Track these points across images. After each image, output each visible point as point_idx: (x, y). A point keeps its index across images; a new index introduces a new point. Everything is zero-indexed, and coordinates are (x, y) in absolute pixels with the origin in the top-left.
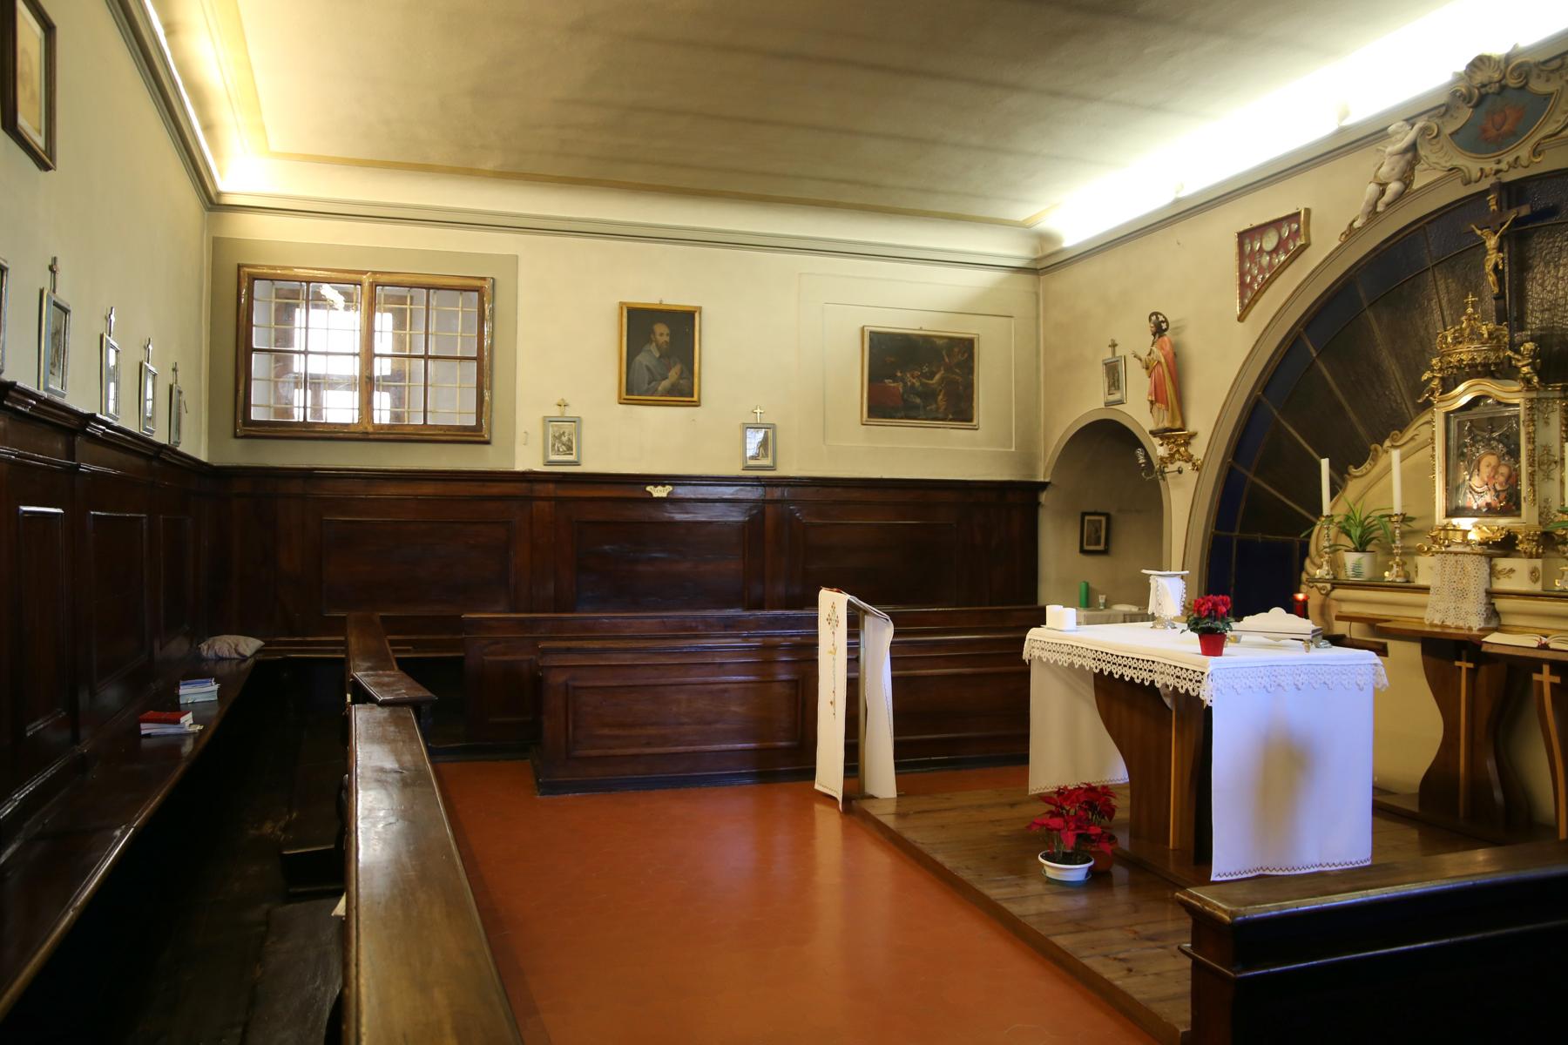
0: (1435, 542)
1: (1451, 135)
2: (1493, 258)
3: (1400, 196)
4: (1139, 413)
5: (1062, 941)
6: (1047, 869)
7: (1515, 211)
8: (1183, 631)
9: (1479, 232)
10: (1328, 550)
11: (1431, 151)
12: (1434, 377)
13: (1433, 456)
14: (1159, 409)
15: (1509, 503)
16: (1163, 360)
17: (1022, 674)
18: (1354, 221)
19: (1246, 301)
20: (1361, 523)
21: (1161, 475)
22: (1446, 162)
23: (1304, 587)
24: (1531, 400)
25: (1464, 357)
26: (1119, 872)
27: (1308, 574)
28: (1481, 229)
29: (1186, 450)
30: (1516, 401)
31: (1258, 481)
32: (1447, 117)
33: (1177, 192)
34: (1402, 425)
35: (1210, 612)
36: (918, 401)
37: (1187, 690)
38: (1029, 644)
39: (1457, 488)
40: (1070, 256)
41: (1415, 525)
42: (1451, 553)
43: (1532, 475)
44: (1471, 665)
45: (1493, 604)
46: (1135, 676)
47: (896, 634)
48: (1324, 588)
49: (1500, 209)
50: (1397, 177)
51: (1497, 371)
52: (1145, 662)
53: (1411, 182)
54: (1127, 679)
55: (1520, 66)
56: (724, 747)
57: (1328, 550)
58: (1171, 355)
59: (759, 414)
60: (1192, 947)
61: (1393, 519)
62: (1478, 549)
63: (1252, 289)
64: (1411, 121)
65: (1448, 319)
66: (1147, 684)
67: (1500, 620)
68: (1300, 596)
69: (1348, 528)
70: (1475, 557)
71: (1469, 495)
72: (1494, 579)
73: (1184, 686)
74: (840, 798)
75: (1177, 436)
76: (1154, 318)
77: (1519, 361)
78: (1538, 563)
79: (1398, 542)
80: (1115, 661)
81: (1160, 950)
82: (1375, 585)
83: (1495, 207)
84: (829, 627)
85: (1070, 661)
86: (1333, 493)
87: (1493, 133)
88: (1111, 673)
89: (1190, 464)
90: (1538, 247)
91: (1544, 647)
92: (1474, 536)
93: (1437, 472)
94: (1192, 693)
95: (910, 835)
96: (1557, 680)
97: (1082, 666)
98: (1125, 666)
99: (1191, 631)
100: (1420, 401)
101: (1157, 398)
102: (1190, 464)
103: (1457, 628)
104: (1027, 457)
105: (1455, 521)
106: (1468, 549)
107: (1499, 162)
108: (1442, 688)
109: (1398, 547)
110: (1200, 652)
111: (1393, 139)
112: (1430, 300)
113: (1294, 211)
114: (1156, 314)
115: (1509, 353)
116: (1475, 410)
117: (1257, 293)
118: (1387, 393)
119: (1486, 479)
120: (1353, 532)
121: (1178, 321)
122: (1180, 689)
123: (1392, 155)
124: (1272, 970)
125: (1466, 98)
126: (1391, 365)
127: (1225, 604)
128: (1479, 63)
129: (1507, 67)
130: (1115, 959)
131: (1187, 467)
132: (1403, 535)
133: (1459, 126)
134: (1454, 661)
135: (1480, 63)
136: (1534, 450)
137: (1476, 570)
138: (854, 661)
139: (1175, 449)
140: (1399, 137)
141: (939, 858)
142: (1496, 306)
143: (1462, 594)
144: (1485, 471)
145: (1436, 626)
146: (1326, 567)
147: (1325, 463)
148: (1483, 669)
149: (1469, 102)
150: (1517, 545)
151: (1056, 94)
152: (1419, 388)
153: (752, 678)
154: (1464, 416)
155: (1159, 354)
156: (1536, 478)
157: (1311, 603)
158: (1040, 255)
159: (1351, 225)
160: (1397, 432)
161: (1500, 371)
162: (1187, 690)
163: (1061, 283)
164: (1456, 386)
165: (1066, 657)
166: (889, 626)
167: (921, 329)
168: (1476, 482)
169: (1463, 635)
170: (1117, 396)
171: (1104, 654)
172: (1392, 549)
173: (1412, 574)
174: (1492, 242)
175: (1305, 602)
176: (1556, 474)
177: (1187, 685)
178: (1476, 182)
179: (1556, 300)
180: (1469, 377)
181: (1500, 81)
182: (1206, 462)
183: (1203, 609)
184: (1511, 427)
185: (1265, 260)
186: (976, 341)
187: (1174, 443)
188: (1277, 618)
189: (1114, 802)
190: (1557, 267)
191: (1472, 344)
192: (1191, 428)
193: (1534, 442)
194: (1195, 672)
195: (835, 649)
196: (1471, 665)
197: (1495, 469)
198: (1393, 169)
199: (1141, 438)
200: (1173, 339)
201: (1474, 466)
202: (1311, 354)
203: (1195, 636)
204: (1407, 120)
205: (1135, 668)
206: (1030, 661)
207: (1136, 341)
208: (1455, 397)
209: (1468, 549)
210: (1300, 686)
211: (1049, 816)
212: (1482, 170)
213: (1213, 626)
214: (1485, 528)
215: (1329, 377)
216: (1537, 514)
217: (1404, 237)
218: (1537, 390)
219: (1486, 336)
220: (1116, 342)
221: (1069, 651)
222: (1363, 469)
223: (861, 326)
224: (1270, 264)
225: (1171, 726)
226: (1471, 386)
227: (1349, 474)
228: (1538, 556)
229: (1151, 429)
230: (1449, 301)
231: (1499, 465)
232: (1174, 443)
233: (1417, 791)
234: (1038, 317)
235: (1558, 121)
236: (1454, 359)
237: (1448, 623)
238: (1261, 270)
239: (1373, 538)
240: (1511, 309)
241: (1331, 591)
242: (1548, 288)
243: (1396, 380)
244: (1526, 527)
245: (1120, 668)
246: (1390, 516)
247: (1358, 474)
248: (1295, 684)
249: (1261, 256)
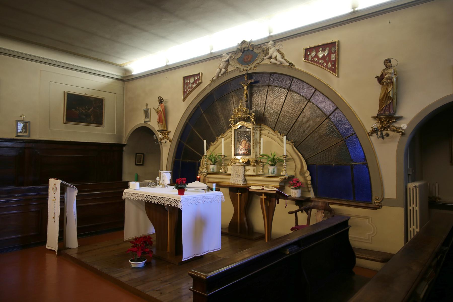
0: (232, 162)
1: (237, 59)
2: (246, 91)
3: (225, 73)
4: (154, 124)
5: (139, 288)
6: (132, 264)
7: (250, 80)
8: (173, 188)
9: (243, 85)
10: (206, 164)
11: (232, 62)
12: (232, 120)
13: (231, 140)
14: (160, 124)
15: (248, 153)
16: (162, 110)
17: (122, 203)
18: (213, 78)
19: (185, 96)
20: (214, 157)
21: (161, 143)
22: (236, 66)
23: (199, 174)
24: (254, 127)
25: (239, 116)
26: (153, 262)
27: (200, 171)
28: (243, 84)
29: (168, 136)
30: (250, 128)
31: (187, 146)
32: (236, 55)
33: (167, 63)
34: (224, 132)
35: (181, 182)
36: (84, 117)
37: (174, 206)
38: (124, 194)
39: (237, 149)
40: (135, 77)
41: (227, 158)
42: (236, 165)
43: (254, 146)
44: (240, 194)
45: (245, 178)
46: (159, 202)
47: (78, 192)
48: (205, 175)
49: (247, 80)
50: (224, 68)
51: (246, 120)
52: (162, 198)
53: (227, 69)
54: (156, 203)
55: (252, 45)
56: (8, 238)
57: (206, 164)
58: (164, 109)
59: (23, 117)
60: (193, 288)
61: (222, 156)
62: (242, 164)
63: (187, 93)
64: (275, 41)
65: (235, 106)
66: (162, 204)
67: (246, 182)
68: (198, 177)
69: (211, 158)
70: (241, 166)
71: (240, 151)
72: (245, 172)
73: (173, 204)
74: (56, 250)
75: (165, 132)
76: (159, 98)
77: (251, 118)
78: (255, 167)
79: (223, 162)
80: (152, 198)
81: (169, 285)
82: (218, 173)
83: (246, 79)
84: (53, 191)
85: (138, 198)
86: (207, 149)
87: (246, 60)
88: (151, 202)
89: (169, 140)
90: (255, 90)
91: (263, 189)
92: (241, 161)
93: (232, 144)
94: (176, 206)
95: (84, 260)
96: (266, 197)
97: (142, 200)
98: (155, 199)
99: (176, 188)
100: (229, 126)
101: (160, 121)
102: (169, 140)
103: (237, 184)
104: (119, 135)
105: (237, 157)
106: (240, 164)
107: (247, 68)
108: (234, 200)
109: (223, 164)
110: (178, 194)
111: (224, 58)
112: (231, 100)
113: (198, 73)
114: (160, 97)
115: (249, 115)
116: (241, 129)
117: (188, 94)
118: (220, 123)
119: (243, 147)
120: (212, 159)
121: (166, 100)
122: (172, 205)
123: (223, 62)
124: (216, 291)
125: (241, 50)
126: (222, 117)
127: (185, 180)
128: (243, 42)
129: (249, 45)
130: (156, 290)
131: (168, 141)
132: (224, 160)
133: (239, 57)
134: (236, 193)
135: (244, 42)
136: (254, 140)
137: (241, 169)
138: (63, 202)
139: (164, 136)
140: (225, 57)
141: (95, 266)
142: (246, 104)
143: (238, 176)
144: (243, 144)
145: (232, 184)
146: (205, 169)
147: (205, 141)
148: (243, 194)
149: (241, 52)
150: (250, 163)
151: (135, 27)
152: (229, 123)
153: (20, 211)
154: (239, 130)
155: (160, 109)
156: (254, 146)
157: (201, 178)
158: (125, 76)
159: (213, 78)
160: (222, 134)
161: (247, 120)
162: (174, 206)
163: (131, 85)
164: (237, 123)
165: (137, 197)
166: (75, 190)
167: (85, 94)
168: (241, 147)
169: (239, 186)
170: (148, 120)
171: (149, 196)
172: (222, 164)
173: (226, 171)
174: (245, 88)
175: (200, 178)
176: (258, 146)
177: (175, 204)
178: (242, 72)
179: (258, 103)
180: (240, 121)
181: (248, 48)
182: (173, 140)
183: (179, 182)
184: (249, 134)
185: (191, 85)
186: (104, 100)
187: (164, 134)
188: (196, 184)
189: (152, 240)
190: (259, 95)
191: (241, 112)
192: (169, 130)
193: (254, 138)
194: (177, 200)
195: (55, 199)
196: (240, 194)
197: (246, 144)
198: (223, 66)
199: (155, 132)
200: (164, 105)
201: (241, 143)
202: (202, 112)
203: (177, 190)
204: (227, 53)
205: (159, 200)
206: (125, 199)
207: (154, 104)
208: (237, 125)
209: (240, 164)
210: (204, 202)
211: (132, 247)
212: (243, 69)
213: (182, 187)
214: (243, 159)
215: (206, 118)
216: (254, 155)
217: (225, 84)
218: (255, 125)
219: (244, 111)
220: (148, 104)
221: (138, 196)
222: (214, 143)
223: (64, 91)
224: (192, 87)
225: (168, 216)
226: (240, 123)
227: (211, 144)
228: (255, 166)
229: (158, 130)
230: (235, 101)
231: (246, 143)
232: (164, 134)
233: (228, 227)
234: (124, 94)
235: (260, 60)
236: (237, 116)
237: (235, 183)
238: (189, 88)
239: (217, 162)
240: (249, 104)
241: (207, 175)
242: (257, 100)
243: (222, 120)
244: (252, 159)
245: (154, 200)
246: (221, 156)
247: (213, 144)
248: (203, 202)
249: (189, 84)
